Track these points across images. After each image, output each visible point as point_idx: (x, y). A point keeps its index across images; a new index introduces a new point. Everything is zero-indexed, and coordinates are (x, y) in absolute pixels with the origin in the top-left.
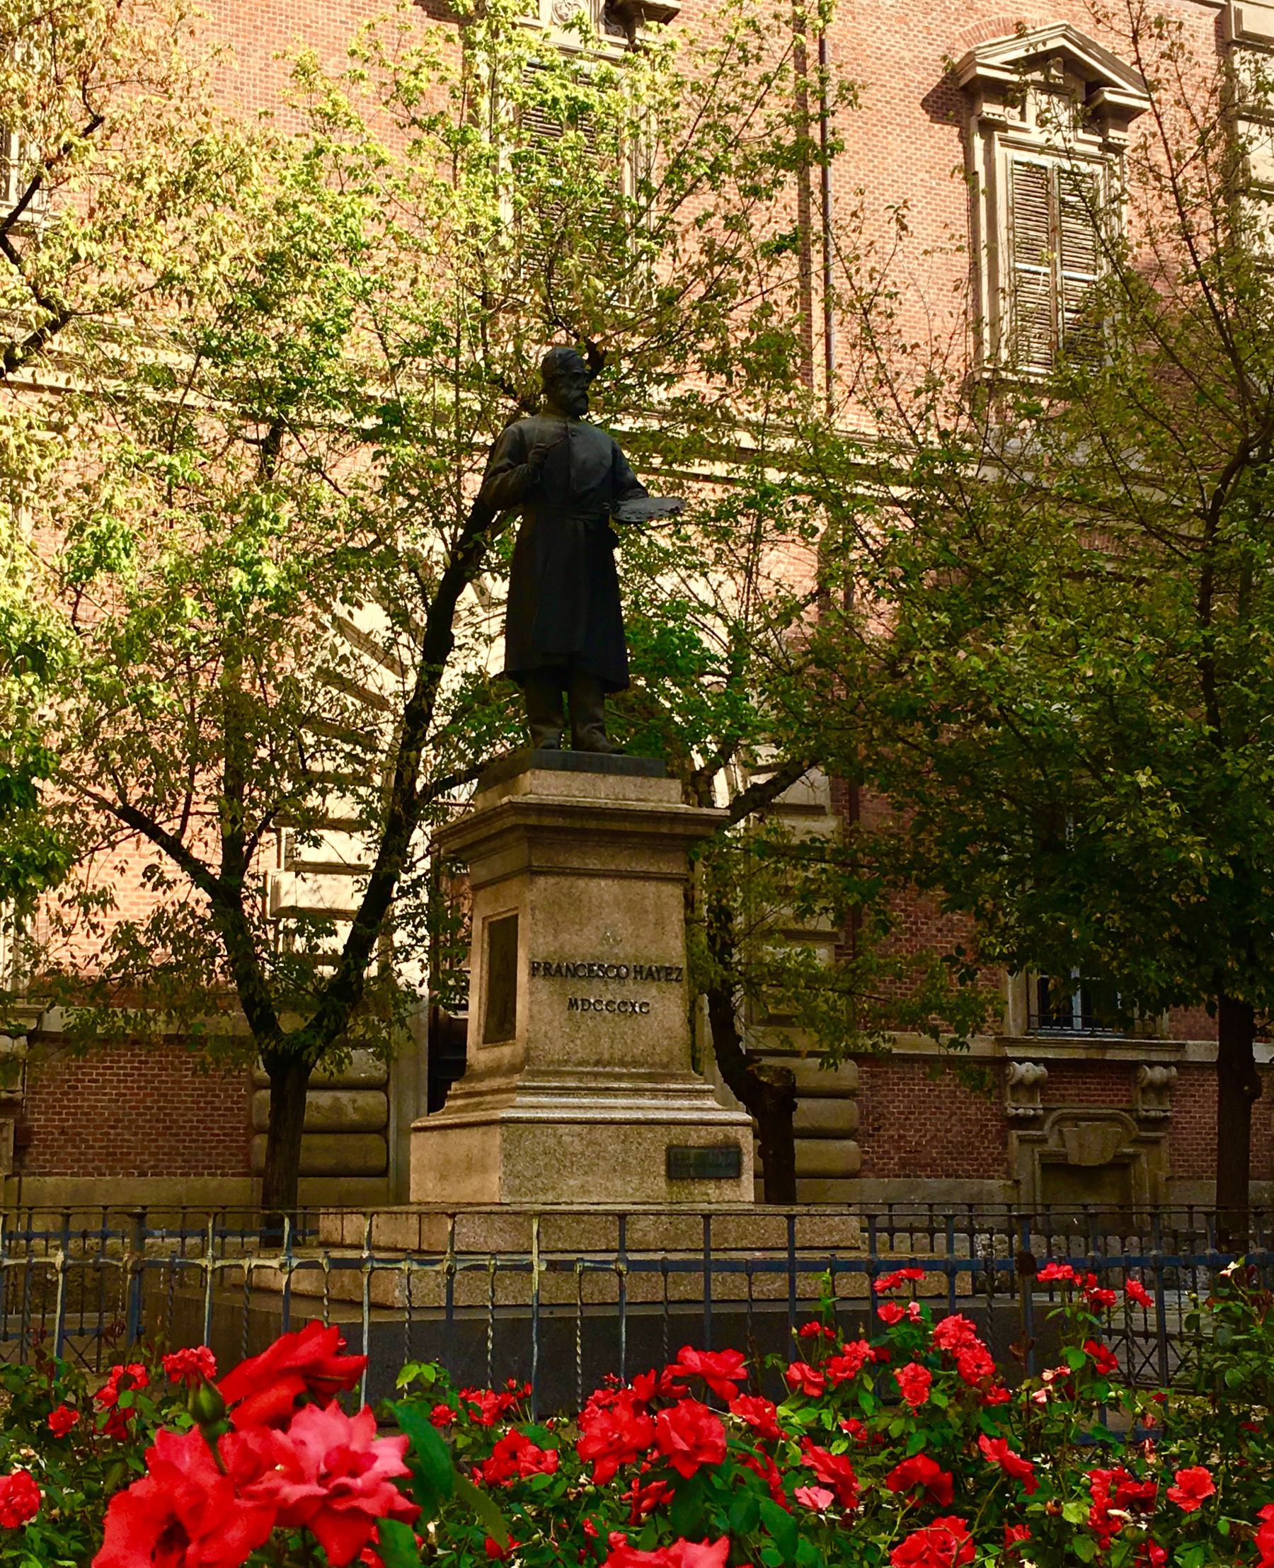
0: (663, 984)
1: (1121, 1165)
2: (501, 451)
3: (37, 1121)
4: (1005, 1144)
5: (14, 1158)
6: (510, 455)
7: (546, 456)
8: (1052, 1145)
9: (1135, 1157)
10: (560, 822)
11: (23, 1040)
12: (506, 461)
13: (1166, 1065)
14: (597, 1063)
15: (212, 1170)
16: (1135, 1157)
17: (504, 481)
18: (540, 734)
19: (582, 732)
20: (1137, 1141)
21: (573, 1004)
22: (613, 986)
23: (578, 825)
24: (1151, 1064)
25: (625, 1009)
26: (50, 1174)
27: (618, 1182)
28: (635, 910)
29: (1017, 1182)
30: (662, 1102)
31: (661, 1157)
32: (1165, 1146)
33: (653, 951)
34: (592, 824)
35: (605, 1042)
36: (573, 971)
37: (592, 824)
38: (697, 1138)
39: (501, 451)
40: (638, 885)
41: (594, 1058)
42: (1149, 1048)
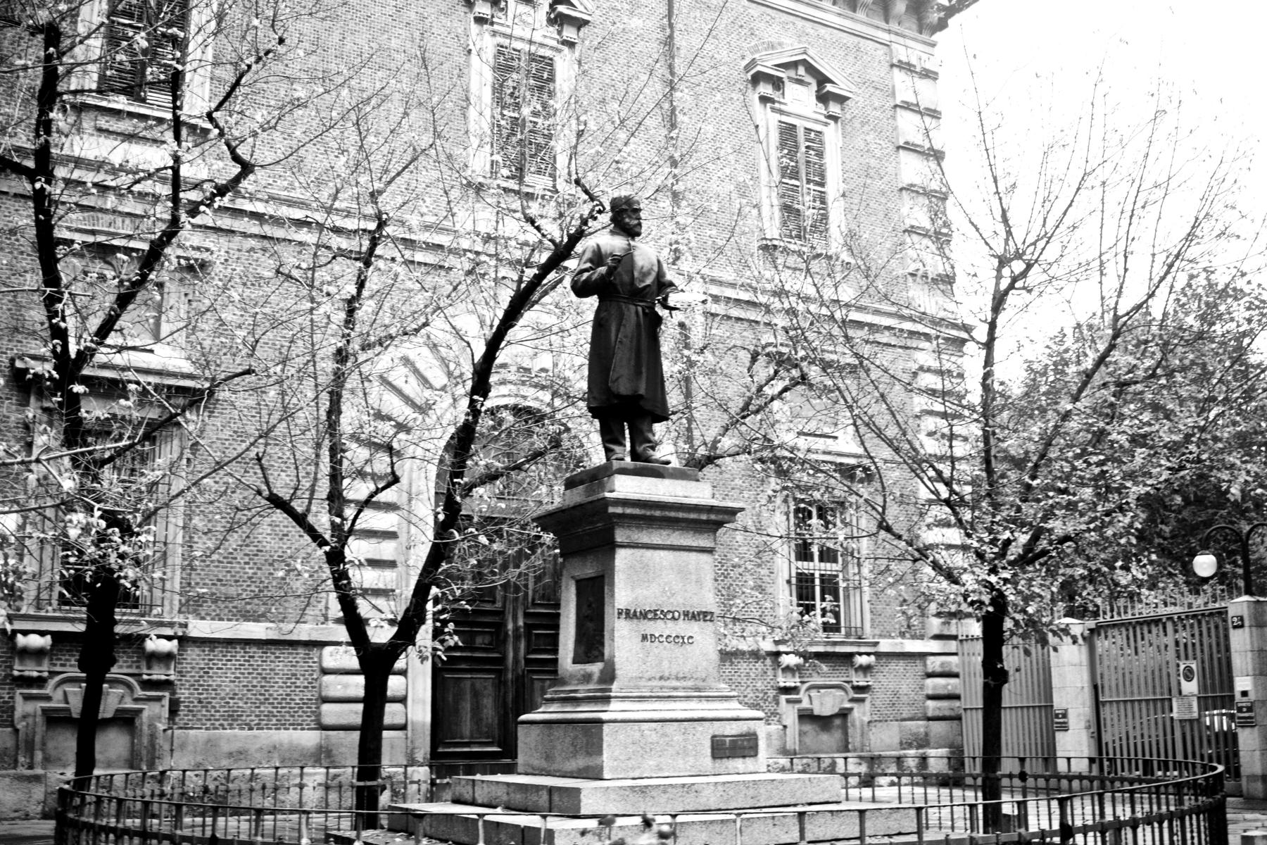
0: (702, 622)
1: (844, 714)
2: (585, 258)
3: (183, 694)
4: (778, 704)
5: (169, 719)
6: (590, 260)
7: (619, 261)
8: (805, 704)
9: (851, 709)
10: (637, 511)
11: (175, 642)
12: (588, 265)
13: (868, 654)
14: (661, 678)
15: (295, 726)
16: (851, 709)
17: (589, 277)
18: (612, 450)
19: (640, 449)
20: (852, 700)
21: (644, 638)
22: (670, 624)
23: (648, 513)
24: (860, 654)
25: (680, 641)
26: (192, 728)
27: (681, 762)
28: (683, 572)
29: (785, 727)
30: (705, 705)
31: (708, 744)
32: (867, 703)
33: (695, 600)
34: (658, 513)
35: (665, 664)
36: (644, 615)
37: (658, 513)
38: (732, 729)
39: (585, 258)
40: (684, 554)
41: (658, 676)
42: (859, 644)
